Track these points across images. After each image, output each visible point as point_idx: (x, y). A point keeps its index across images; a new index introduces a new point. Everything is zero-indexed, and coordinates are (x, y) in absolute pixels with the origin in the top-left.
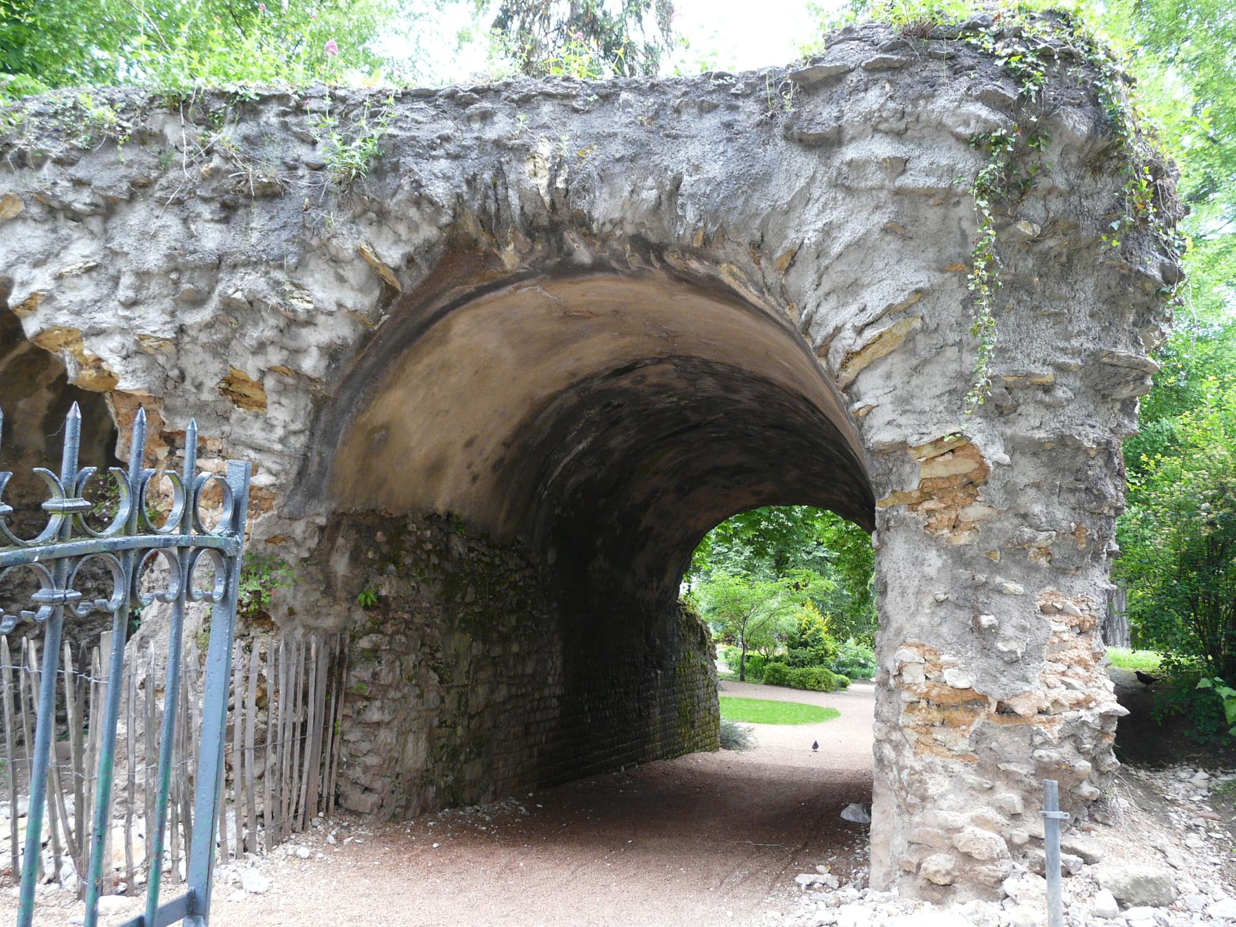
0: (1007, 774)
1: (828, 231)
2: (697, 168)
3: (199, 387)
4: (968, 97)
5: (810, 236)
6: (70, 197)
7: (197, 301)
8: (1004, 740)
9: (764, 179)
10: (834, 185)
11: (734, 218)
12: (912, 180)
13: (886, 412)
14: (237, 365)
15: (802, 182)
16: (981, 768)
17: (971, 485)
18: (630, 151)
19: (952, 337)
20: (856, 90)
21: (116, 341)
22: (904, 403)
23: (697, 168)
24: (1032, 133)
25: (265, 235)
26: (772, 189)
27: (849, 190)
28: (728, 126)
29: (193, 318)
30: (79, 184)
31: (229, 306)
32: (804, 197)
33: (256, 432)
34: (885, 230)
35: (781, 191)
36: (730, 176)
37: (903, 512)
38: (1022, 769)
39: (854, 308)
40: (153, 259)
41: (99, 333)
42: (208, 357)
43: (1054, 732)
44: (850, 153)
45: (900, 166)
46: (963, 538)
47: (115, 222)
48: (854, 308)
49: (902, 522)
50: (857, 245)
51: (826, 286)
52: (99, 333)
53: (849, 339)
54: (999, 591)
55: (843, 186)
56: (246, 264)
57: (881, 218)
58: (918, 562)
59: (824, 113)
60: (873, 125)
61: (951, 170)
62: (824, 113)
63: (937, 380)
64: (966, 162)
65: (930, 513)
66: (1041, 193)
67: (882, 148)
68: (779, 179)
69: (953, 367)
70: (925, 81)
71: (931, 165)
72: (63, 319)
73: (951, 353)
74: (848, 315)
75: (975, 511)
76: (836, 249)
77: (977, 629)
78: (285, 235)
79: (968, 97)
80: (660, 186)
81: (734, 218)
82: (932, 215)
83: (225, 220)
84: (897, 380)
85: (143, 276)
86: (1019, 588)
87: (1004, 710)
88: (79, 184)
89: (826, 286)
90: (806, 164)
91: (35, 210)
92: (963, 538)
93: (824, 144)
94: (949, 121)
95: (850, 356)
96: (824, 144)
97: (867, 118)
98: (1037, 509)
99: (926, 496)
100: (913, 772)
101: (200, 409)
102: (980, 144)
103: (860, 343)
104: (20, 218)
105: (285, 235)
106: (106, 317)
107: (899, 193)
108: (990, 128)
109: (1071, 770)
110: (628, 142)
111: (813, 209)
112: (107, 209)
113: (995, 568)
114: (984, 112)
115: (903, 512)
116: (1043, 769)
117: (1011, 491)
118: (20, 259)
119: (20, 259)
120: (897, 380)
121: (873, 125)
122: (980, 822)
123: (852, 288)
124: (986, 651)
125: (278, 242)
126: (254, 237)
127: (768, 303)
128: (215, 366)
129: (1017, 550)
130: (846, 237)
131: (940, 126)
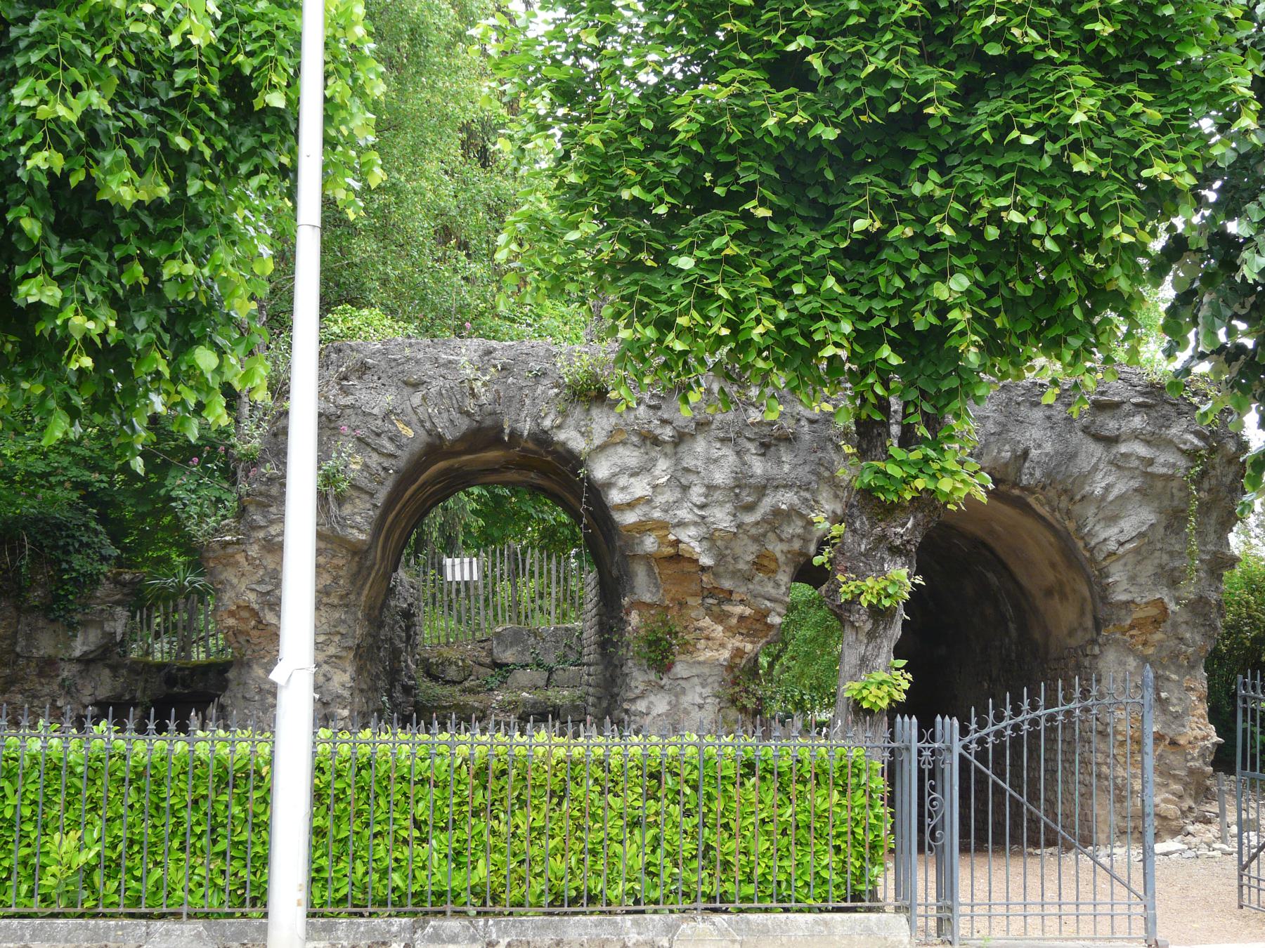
0: (1174, 776)
1: (1107, 488)
2: (1039, 446)
3: (736, 559)
4: (1186, 431)
5: (1098, 491)
6: (658, 431)
7: (750, 508)
8: (1173, 759)
9: (1073, 456)
10: (1111, 463)
11: (1059, 477)
12: (1158, 469)
13: (1124, 585)
14: (770, 548)
15: (1094, 460)
16: (1161, 774)
17: (1157, 622)
18: (998, 429)
19: (1159, 546)
20: (1128, 415)
21: (692, 531)
22: (1132, 579)
23: (1039, 446)
24: (1212, 450)
25: (795, 467)
26: (1078, 461)
27: (1119, 467)
28: (1049, 418)
29: (749, 519)
30: (664, 422)
31: (776, 512)
32: (1095, 468)
33: (769, 589)
34: (1136, 490)
35: (1084, 463)
36: (1057, 453)
37: (1118, 636)
38: (1182, 773)
39: (1116, 530)
40: (721, 477)
41: (681, 524)
42: (749, 542)
43: (1196, 753)
44: (1123, 448)
45: (1151, 462)
46: (1150, 651)
47: (683, 448)
48: (1116, 530)
49: (1116, 641)
50: (1120, 497)
51: (1101, 516)
52: (681, 524)
53: (1112, 546)
54: (1168, 679)
55: (1118, 464)
56: (785, 486)
57: (1135, 484)
58: (1122, 663)
59: (1111, 425)
60: (1136, 436)
61: (1174, 465)
62: (1111, 425)
63: (1149, 568)
64: (1182, 462)
65: (1132, 637)
66: (695, 92)
67: (1141, 450)
68: (1082, 456)
69: (1156, 562)
70: (1164, 416)
71: (1166, 461)
72: (657, 514)
73: (1157, 554)
74: (1112, 532)
75: (1158, 636)
76: (1111, 497)
77: (1159, 699)
78: (807, 468)
79: (1186, 431)
80: (1014, 451)
81: (1059, 477)
82: (1159, 484)
83: (763, 455)
84: (1129, 567)
85: (711, 488)
86: (1174, 677)
87: (1173, 743)
88: (664, 422)
89: (1101, 516)
90: (1097, 450)
91: (635, 439)
92: (1150, 651)
93: (1110, 441)
94: (1176, 441)
95: (1111, 554)
96: (1110, 441)
97: (1134, 431)
98: (1188, 635)
99: (1132, 627)
100: (1124, 779)
101: (734, 574)
102: (1192, 455)
103: (1121, 550)
104: (624, 443)
105: (807, 468)
106: (683, 514)
107: (1146, 474)
108: (1197, 450)
109: (1203, 772)
110: (997, 423)
111: (1099, 475)
112: (681, 438)
113: (1165, 668)
114: (1196, 441)
115: (1118, 636)
116: (1191, 772)
117: (1175, 626)
118: (622, 471)
119: (622, 471)
120: (1129, 567)
121: (1136, 436)
122: (1166, 801)
123: (1112, 519)
124: (1165, 711)
125: (803, 473)
126: (786, 468)
127: (1055, 518)
128: (754, 548)
129: (1175, 656)
130: (1115, 492)
131: (1171, 441)
